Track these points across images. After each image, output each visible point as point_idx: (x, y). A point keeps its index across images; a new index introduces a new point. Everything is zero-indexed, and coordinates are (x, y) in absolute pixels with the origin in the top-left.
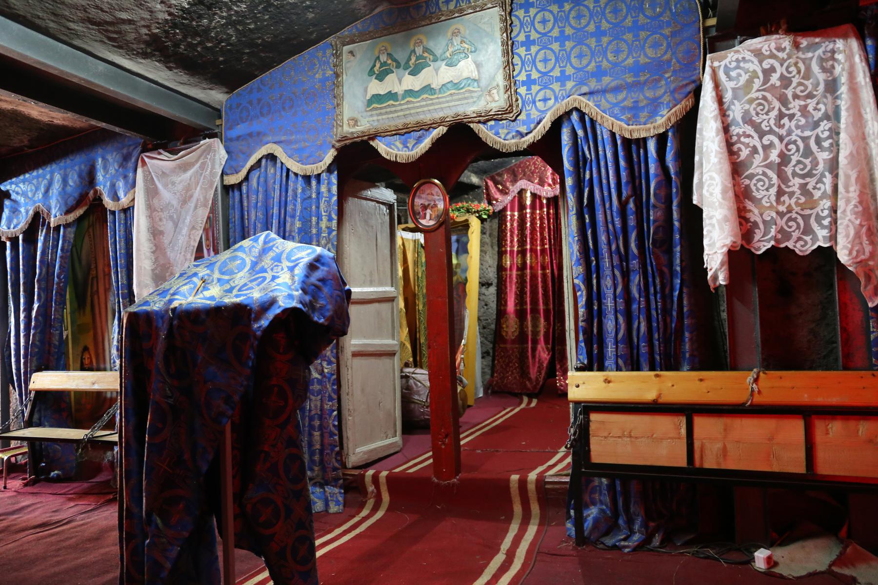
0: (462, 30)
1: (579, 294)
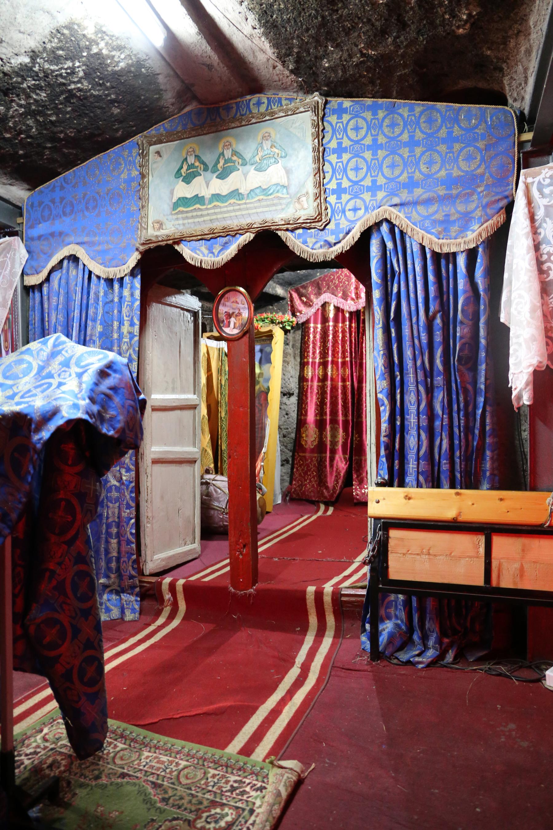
0: (273, 134)
1: (382, 408)
